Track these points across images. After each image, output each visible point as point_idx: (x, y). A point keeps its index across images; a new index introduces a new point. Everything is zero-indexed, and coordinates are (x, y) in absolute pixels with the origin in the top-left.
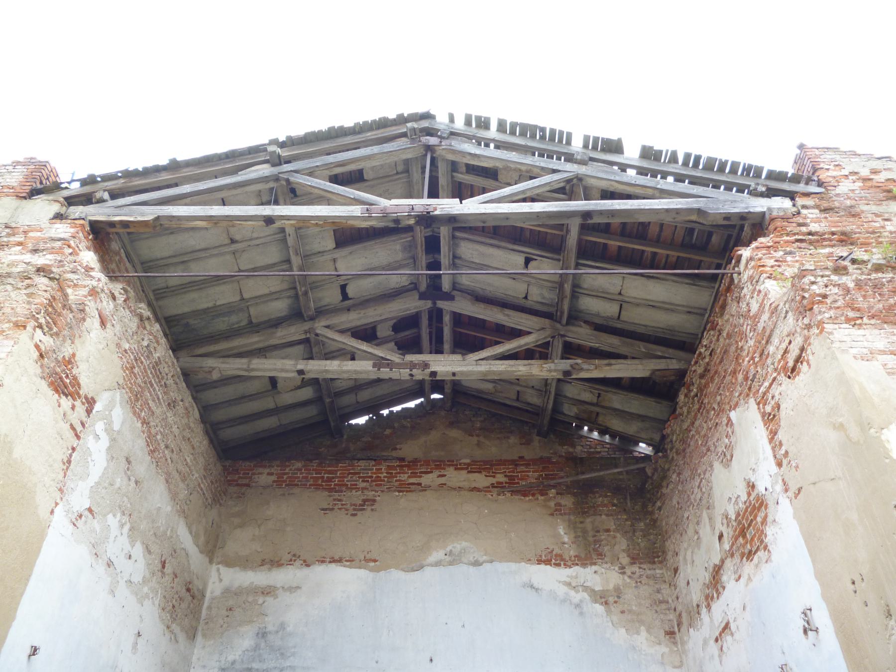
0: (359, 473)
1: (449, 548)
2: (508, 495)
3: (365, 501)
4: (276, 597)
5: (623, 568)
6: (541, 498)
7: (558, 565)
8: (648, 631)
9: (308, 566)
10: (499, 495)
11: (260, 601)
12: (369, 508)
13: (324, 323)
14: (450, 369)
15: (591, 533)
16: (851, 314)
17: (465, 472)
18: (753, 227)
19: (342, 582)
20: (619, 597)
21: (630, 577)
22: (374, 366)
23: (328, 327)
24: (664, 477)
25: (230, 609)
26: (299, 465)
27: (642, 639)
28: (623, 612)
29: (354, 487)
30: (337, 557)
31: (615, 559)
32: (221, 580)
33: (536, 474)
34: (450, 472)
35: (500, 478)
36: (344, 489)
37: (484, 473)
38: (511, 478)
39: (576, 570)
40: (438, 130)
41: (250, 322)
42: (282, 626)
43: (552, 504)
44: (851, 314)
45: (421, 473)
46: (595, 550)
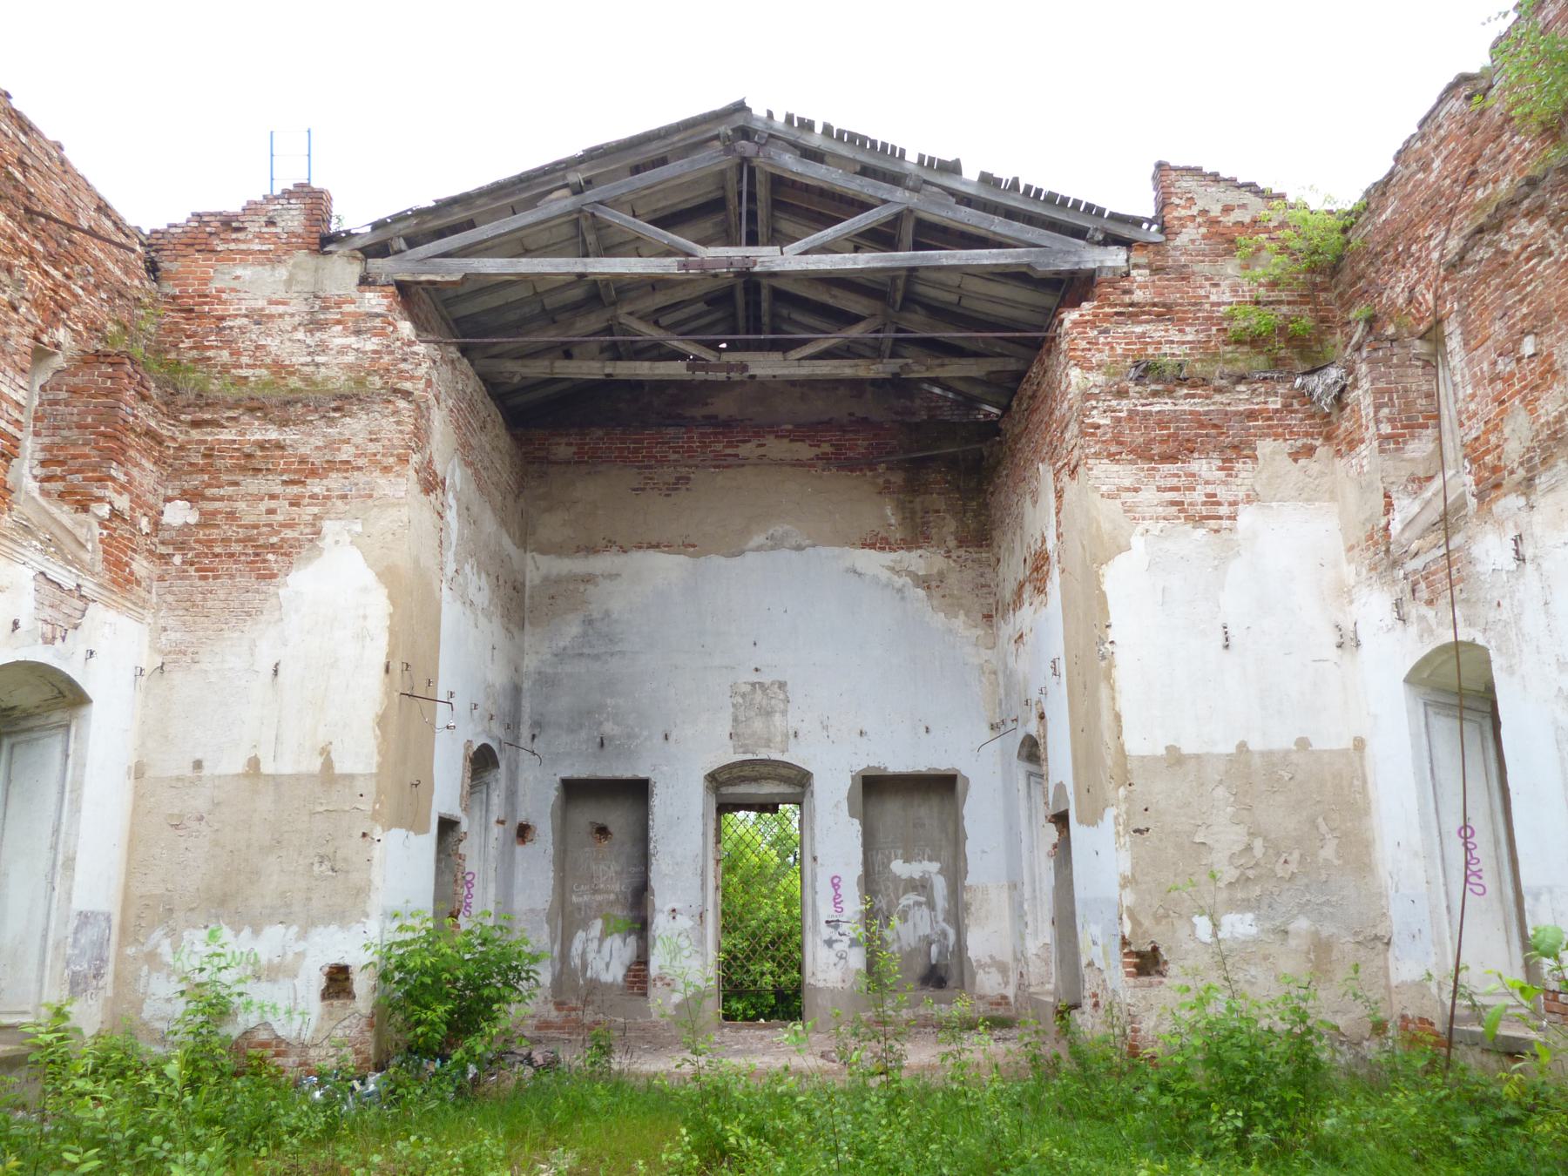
3: (678, 479)
4: (596, 585)
6: (869, 474)
7: (882, 549)
13: (627, 309)
14: (770, 372)
15: (920, 514)
22: (688, 368)
23: (631, 314)
24: (999, 463)
26: (600, 433)
27: (959, 622)
29: (662, 461)
33: (866, 443)
34: (770, 440)
35: (826, 448)
40: (756, 131)
41: (544, 309)
42: (607, 614)
43: (881, 481)
44: (1113, 449)
46: (922, 533)
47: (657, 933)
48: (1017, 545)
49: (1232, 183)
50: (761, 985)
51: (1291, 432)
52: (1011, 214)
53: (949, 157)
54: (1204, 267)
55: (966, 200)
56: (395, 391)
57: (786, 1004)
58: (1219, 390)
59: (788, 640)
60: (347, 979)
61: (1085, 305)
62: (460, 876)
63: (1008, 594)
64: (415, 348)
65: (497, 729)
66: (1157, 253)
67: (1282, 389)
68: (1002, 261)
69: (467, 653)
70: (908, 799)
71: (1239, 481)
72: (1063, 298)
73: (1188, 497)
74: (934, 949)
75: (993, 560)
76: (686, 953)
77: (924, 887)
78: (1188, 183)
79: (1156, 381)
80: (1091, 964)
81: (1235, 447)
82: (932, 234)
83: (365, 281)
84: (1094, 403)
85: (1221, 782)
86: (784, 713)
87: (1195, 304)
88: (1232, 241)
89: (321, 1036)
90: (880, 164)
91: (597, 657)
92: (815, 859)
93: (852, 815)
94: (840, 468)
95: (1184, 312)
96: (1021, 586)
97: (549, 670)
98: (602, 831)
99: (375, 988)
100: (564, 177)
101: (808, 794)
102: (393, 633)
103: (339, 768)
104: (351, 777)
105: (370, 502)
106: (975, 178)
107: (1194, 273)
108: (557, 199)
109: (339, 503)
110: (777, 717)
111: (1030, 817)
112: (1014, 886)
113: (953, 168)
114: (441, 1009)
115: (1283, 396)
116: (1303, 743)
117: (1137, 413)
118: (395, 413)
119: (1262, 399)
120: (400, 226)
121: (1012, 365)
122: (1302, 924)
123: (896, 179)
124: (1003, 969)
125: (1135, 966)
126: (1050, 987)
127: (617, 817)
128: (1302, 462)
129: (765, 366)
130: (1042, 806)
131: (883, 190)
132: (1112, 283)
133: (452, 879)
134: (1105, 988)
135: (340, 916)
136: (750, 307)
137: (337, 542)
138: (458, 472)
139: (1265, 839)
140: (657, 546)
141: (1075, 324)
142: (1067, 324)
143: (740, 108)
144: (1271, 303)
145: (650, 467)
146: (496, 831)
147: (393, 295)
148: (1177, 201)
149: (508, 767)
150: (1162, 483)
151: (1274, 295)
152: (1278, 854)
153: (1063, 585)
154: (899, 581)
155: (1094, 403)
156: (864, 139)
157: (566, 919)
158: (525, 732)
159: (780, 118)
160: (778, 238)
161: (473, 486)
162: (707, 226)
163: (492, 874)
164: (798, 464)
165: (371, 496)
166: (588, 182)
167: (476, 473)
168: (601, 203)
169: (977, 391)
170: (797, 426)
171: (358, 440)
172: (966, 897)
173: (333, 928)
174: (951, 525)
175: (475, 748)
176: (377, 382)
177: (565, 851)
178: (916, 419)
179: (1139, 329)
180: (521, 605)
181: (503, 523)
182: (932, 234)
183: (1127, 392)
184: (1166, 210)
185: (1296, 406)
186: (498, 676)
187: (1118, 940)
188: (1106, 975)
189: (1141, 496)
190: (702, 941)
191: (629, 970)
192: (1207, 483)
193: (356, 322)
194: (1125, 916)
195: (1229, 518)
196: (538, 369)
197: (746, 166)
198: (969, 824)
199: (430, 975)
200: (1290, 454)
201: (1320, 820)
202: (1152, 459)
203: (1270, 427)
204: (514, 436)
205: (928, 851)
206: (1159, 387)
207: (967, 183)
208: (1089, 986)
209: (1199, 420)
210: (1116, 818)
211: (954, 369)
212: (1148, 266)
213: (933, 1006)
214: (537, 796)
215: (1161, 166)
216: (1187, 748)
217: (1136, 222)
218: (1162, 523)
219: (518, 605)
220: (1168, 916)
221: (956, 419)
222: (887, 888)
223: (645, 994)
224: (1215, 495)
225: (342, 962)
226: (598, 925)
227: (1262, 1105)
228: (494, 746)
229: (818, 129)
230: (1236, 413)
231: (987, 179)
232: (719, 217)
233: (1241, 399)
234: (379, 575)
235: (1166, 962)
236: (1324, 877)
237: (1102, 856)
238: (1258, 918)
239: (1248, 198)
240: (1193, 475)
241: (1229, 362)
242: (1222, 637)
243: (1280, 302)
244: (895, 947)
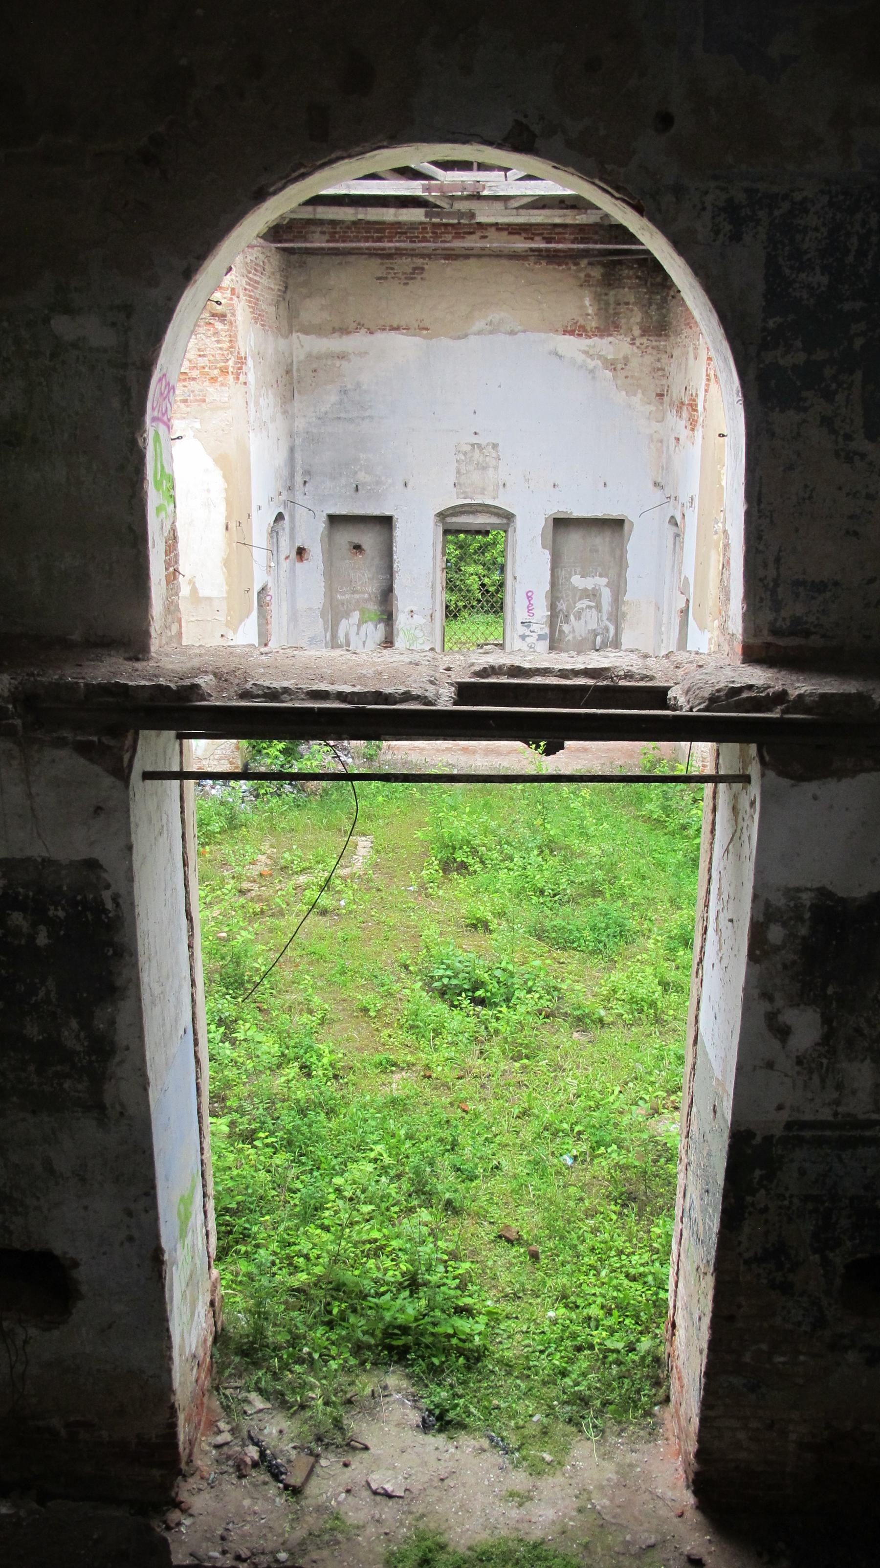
0: (405, 233)
3: (415, 269)
4: (349, 361)
5: (633, 339)
7: (580, 335)
8: (643, 394)
9: (371, 333)
10: (535, 263)
12: (419, 277)
15: (612, 306)
19: (402, 347)
22: (427, 215)
27: (637, 400)
28: (626, 377)
30: (395, 326)
37: (524, 235)
42: (358, 385)
46: (614, 322)
47: (401, 626)
76: (421, 641)
77: (594, 595)
86: (496, 468)
89: (208, 754)
91: (351, 420)
93: (544, 547)
97: (315, 430)
102: (229, 503)
103: (203, 593)
104: (209, 599)
105: (203, 405)
109: (182, 405)
110: (491, 472)
118: (216, 333)
127: (369, 539)
140: (397, 329)
154: (591, 364)
158: (299, 479)
164: (515, 256)
165: (204, 401)
172: (624, 608)
174: (637, 316)
177: (331, 565)
205: (600, 569)
210: (710, 640)
214: (311, 530)
222: (567, 596)
226: (356, 615)
234: (216, 461)
244: (570, 637)
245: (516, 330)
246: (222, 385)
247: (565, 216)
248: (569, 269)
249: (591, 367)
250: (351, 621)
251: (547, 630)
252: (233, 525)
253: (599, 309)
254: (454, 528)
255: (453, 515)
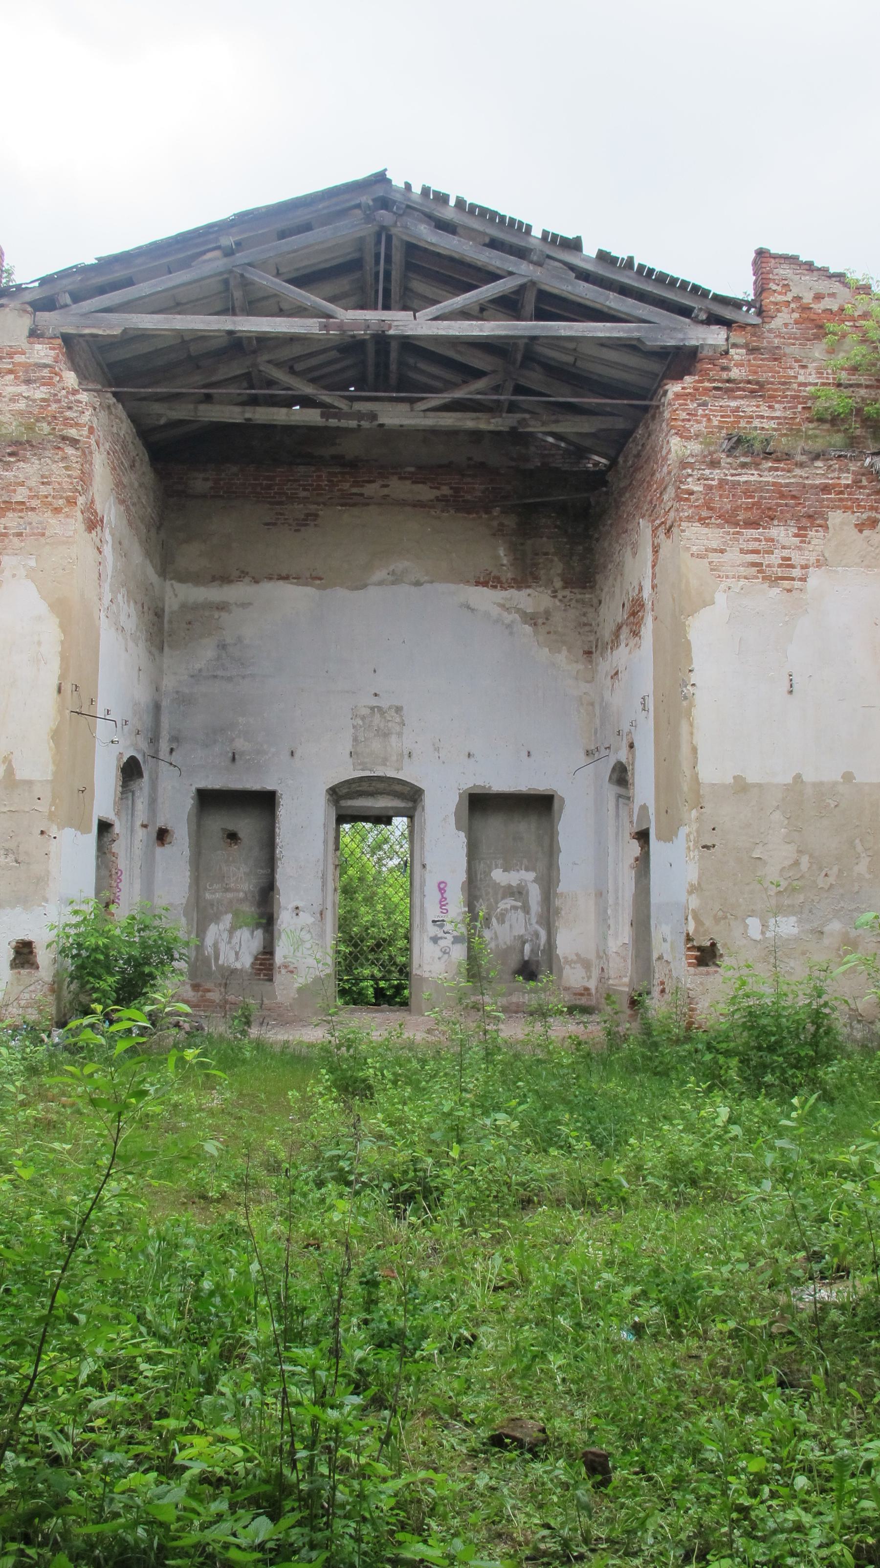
0: (298, 481)
1: (391, 568)
2: (452, 512)
3: (308, 515)
4: (230, 612)
5: (555, 591)
6: (485, 516)
7: (495, 587)
8: (569, 651)
9: (257, 582)
10: (443, 511)
11: (216, 616)
12: (312, 523)
13: (266, 357)
16: (704, 513)
17: (408, 482)
18: (682, 361)
19: (292, 598)
20: (547, 619)
21: (560, 601)
22: (323, 415)
23: (269, 362)
25: (190, 623)
26: (235, 469)
27: (562, 658)
28: (549, 633)
29: (292, 498)
30: (284, 574)
31: (550, 582)
32: (176, 595)
34: (394, 482)
35: (446, 491)
36: (284, 499)
37: (429, 484)
38: (456, 490)
39: (512, 592)
40: (394, 202)
42: (240, 640)
43: (495, 523)
44: (704, 513)
45: (364, 481)
46: (532, 573)
47: (283, 926)
48: (617, 591)
49: (825, 273)
50: (373, 973)
51: (859, 506)
52: (624, 291)
53: (570, 234)
54: (793, 350)
55: (585, 276)
56: (64, 438)
57: (392, 995)
58: (801, 465)
59: (405, 668)
60: (31, 952)
61: (687, 379)
62: (114, 871)
63: (607, 633)
64: (78, 397)
65: (143, 745)
66: (754, 335)
67: (853, 467)
68: (615, 334)
69: (119, 672)
70: (509, 814)
71: (811, 547)
72: (668, 368)
73: (767, 560)
74: (527, 947)
75: (595, 601)
76: (308, 945)
77: (520, 893)
78: (784, 271)
79: (745, 455)
80: (660, 958)
81: (810, 517)
82: (551, 306)
83: (34, 334)
84: (690, 471)
85: (778, 807)
86: (400, 735)
87: (784, 383)
88: (821, 327)
90: (507, 236)
91: (230, 679)
92: (424, 866)
94: (458, 510)
95: (776, 390)
96: (619, 627)
97: (186, 690)
98: (233, 837)
99: (55, 961)
100: (217, 240)
101: (419, 809)
102: (64, 658)
104: (29, 783)
105: (42, 539)
106: (593, 254)
107: (785, 355)
108: (210, 260)
110: (393, 739)
111: (617, 834)
112: (600, 894)
113: (575, 245)
114: (111, 980)
115: (854, 473)
116: (848, 777)
117: (727, 482)
118: (64, 459)
119: (836, 474)
120: (65, 282)
121: (620, 424)
122: (835, 926)
123: (521, 253)
124: (587, 965)
125: (696, 958)
126: (626, 980)
127: (246, 825)
128: (866, 532)
129: (394, 416)
130: (627, 825)
131: (508, 263)
132: (712, 360)
133: (108, 874)
134: (671, 977)
135: (23, 900)
136: (382, 365)
137: (14, 576)
138: (113, 511)
139: (811, 856)
141: (678, 396)
142: (670, 395)
143: (381, 179)
144: (851, 386)
145: (280, 503)
146: (140, 833)
147: (60, 348)
148: (774, 287)
149: (150, 777)
150: (744, 546)
151: (854, 379)
152: (821, 869)
153: (655, 632)
154: (508, 618)
155: (690, 471)
156: (494, 214)
157: (202, 914)
159: (417, 190)
160: (409, 302)
161: (125, 522)
162: (343, 284)
163: (137, 871)
164: (419, 505)
165: (43, 535)
166: (238, 244)
167: (127, 509)
168: (250, 265)
169: (587, 443)
170: (420, 468)
171: (32, 483)
172: (558, 902)
173: (19, 909)
174: (558, 567)
175: (125, 760)
176: (45, 428)
178: (530, 466)
179: (733, 404)
180: (161, 630)
181: (148, 554)
182: (551, 306)
183: (719, 462)
184: (764, 295)
185: (865, 482)
186: (142, 695)
187: (683, 937)
188: (672, 966)
189: (727, 557)
190: (322, 935)
191: (256, 959)
192: (784, 547)
193: (27, 372)
194: (690, 918)
195: (801, 579)
196: (181, 412)
197: (383, 234)
198: (563, 839)
199: (102, 953)
200: (856, 525)
201: (857, 841)
202: (737, 524)
203: (841, 500)
204: (156, 471)
205: (525, 861)
206: (748, 460)
207: (587, 259)
208: (659, 975)
209: (780, 491)
211: (571, 426)
212: (746, 346)
213: (527, 994)
214: (176, 807)
215: (761, 254)
216: (752, 778)
217: (736, 304)
218: (743, 582)
219: (161, 631)
220: (726, 918)
221: (566, 467)
222: (487, 894)
223: (271, 980)
224: (789, 559)
225: (26, 938)
226: (228, 919)
227: (781, 1059)
228: (140, 757)
229: (452, 202)
230: (813, 486)
231: (604, 257)
232: (357, 275)
233: (818, 474)
234: (51, 606)
235: (721, 956)
236: (856, 889)
237: (676, 866)
238: (799, 921)
239: (836, 287)
240: (772, 540)
241: (808, 437)
242: (788, 684)
243: (859, 386)
245: (422, 580)
246: (67, 516)
247: (478, 418)
248: (481, 517)
249: (507, 621)
250: (222, 926)
251: (463, 929)
252: (67, 688)
253: (516, 559)
254: (349, 812)
255: (350, 796)
